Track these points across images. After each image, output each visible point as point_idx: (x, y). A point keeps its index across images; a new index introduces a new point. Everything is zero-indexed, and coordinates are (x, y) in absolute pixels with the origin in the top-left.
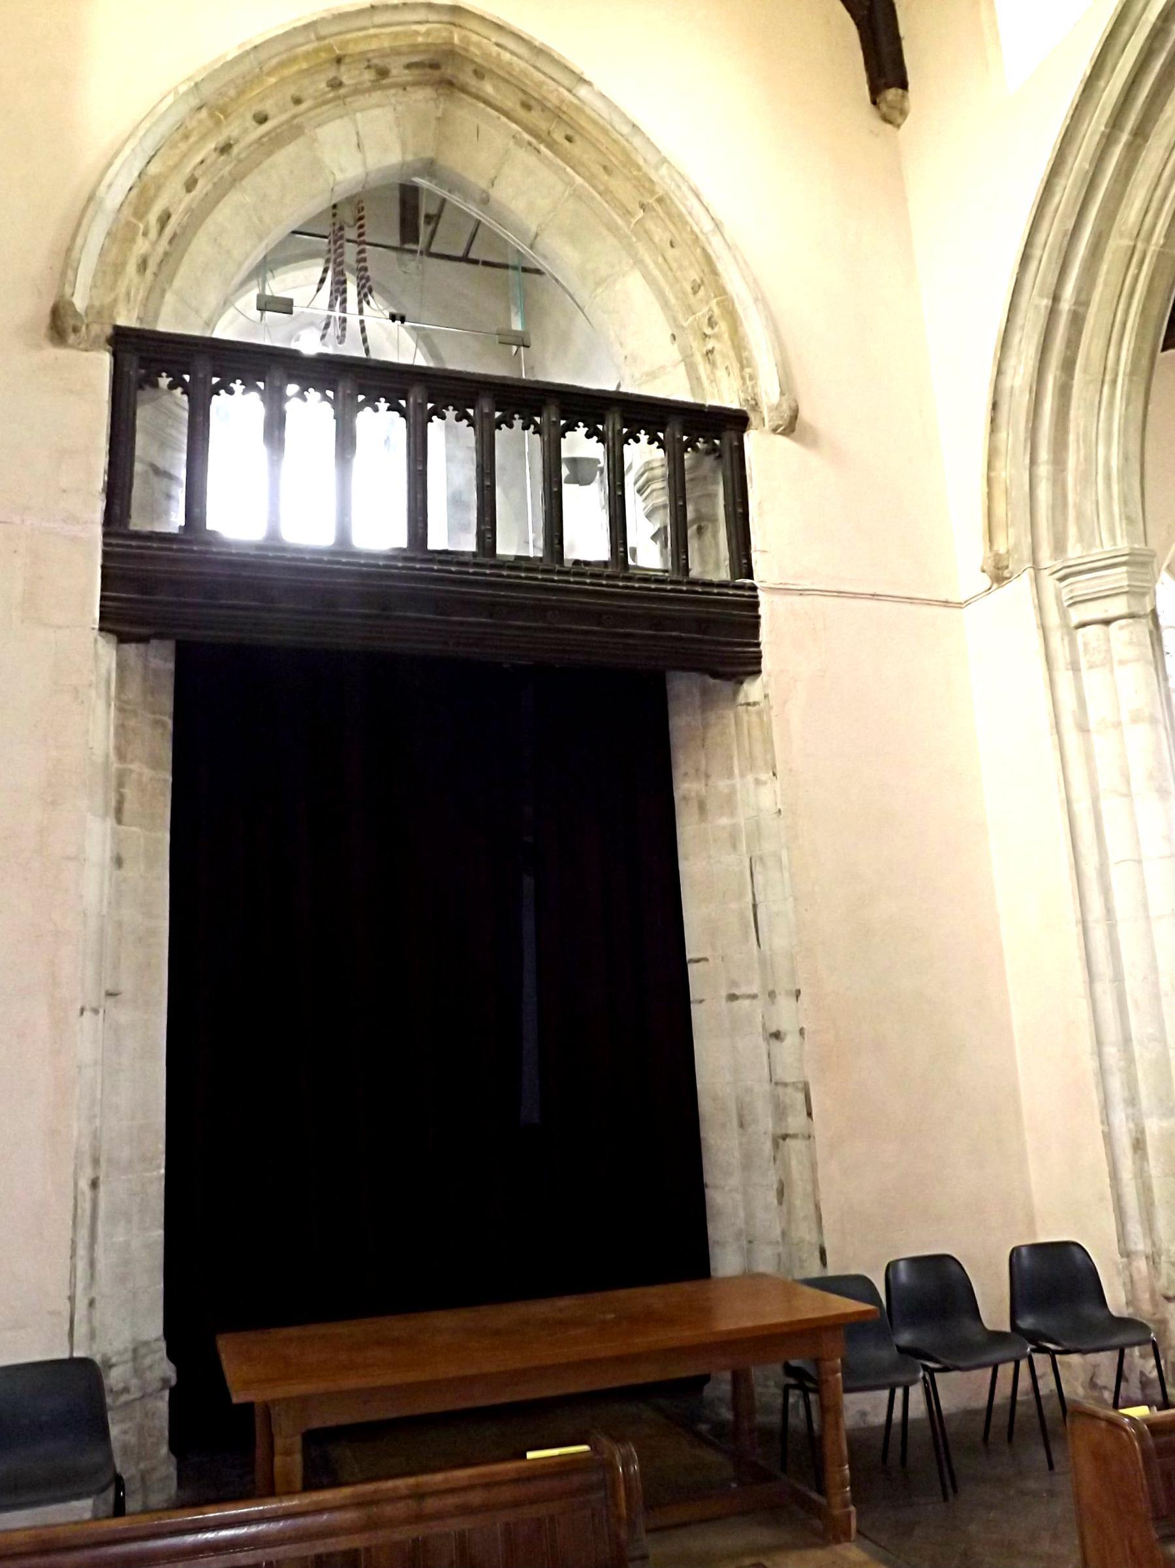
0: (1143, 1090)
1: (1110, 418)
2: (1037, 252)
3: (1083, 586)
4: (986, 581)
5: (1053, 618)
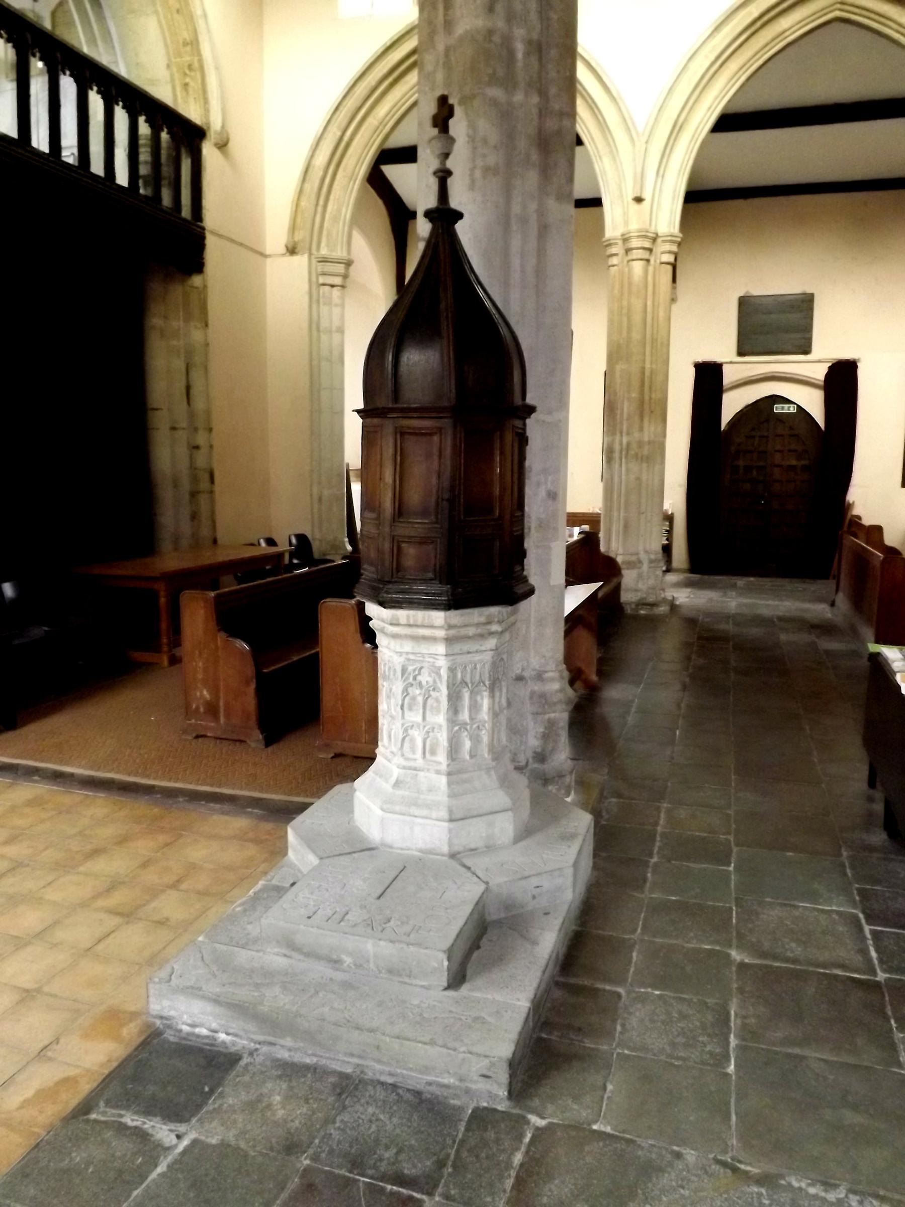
3: (329, 267)
4: (284, 250)
5: (314, 279)
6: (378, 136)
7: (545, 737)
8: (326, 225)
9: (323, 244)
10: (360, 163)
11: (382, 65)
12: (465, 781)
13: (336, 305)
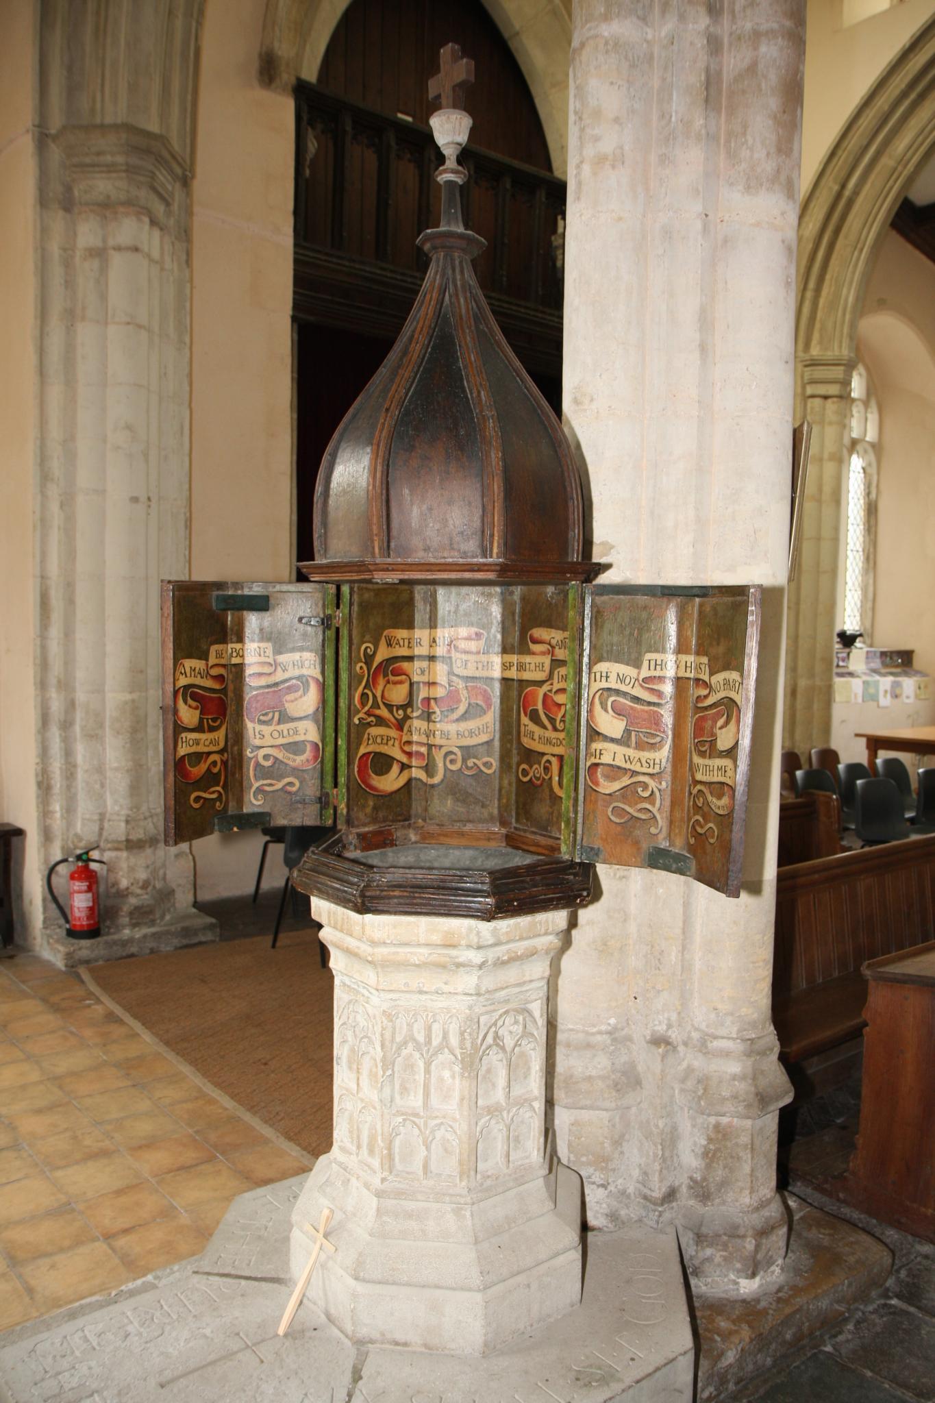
0: (801, 664)
1: (854, 273)
2: (840, 152)
3: (820, 373)
6: (895, 182)
7: (710, 1156)
8: (819, 314)
9: (814, 342)
10: (868, 225)
11: (898, 79)
12: (409, 1215)
13: (830, 423)
